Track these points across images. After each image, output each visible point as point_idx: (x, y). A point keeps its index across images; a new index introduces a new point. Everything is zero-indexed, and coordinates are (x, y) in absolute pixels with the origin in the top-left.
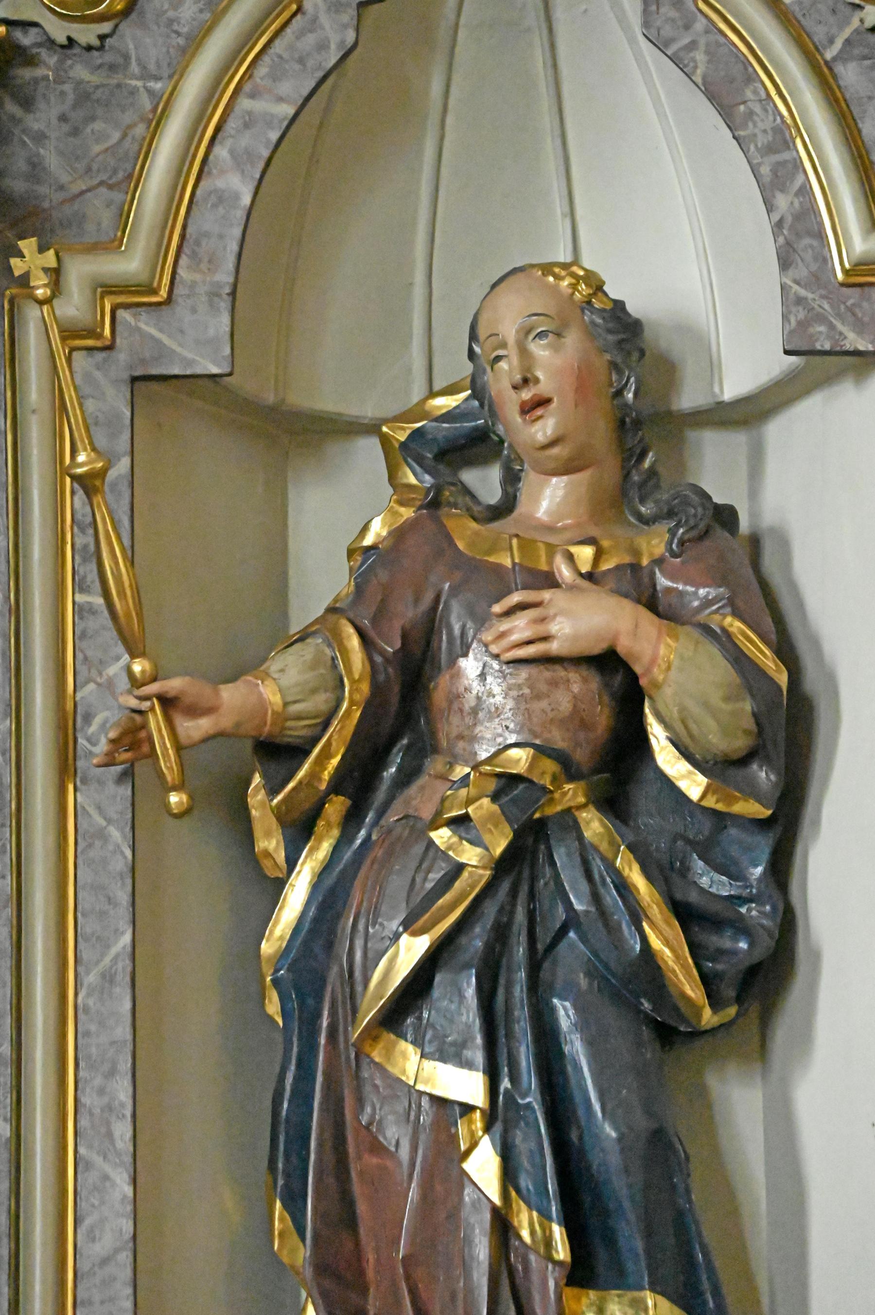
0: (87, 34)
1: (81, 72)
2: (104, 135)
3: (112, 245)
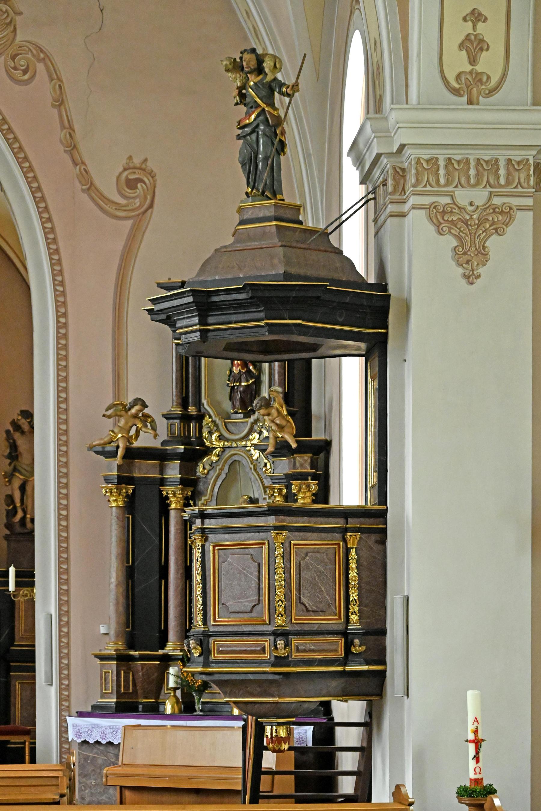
0: (204, 476)
1: (204, 479)
2: (206, 485)
3: (206, 496)
